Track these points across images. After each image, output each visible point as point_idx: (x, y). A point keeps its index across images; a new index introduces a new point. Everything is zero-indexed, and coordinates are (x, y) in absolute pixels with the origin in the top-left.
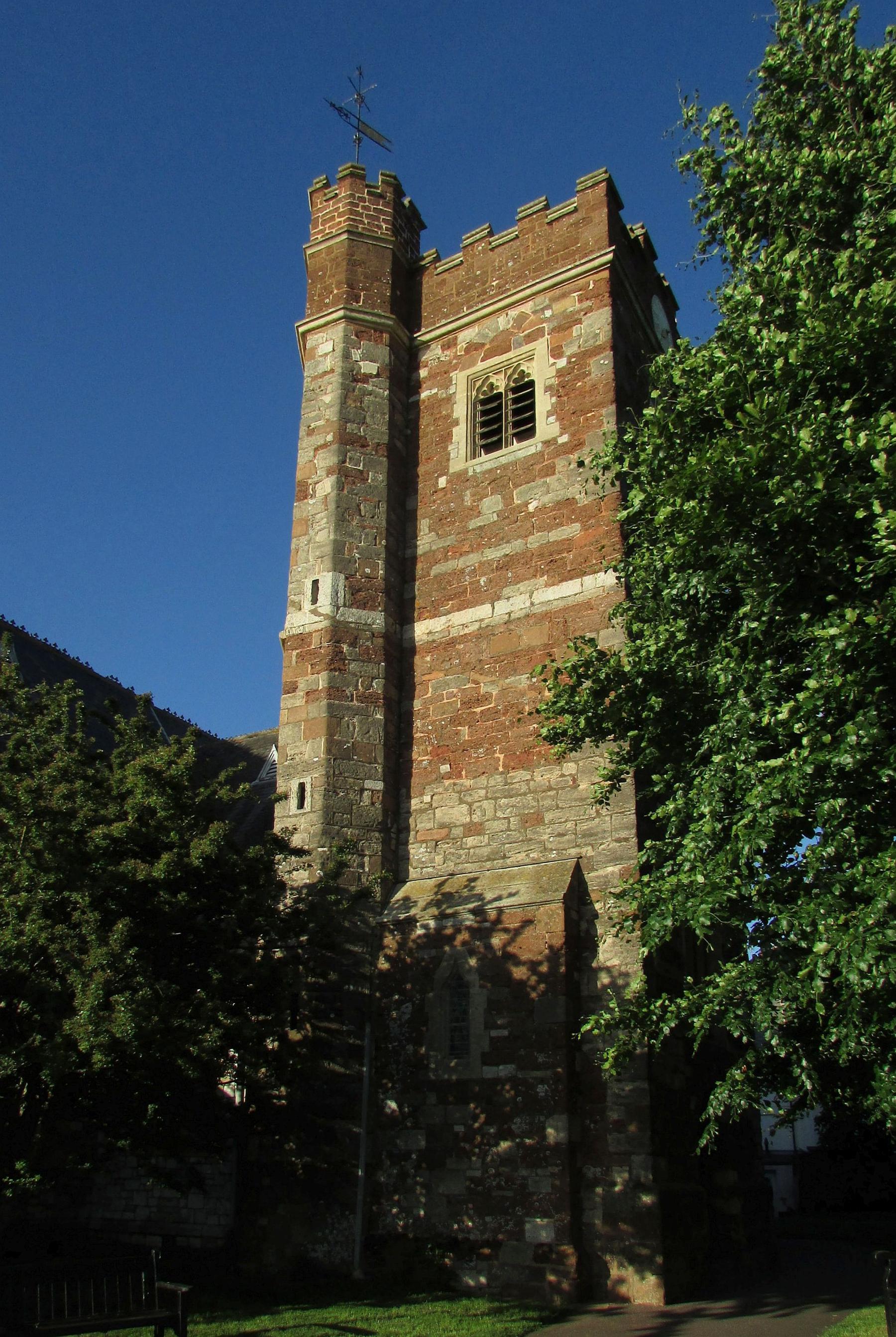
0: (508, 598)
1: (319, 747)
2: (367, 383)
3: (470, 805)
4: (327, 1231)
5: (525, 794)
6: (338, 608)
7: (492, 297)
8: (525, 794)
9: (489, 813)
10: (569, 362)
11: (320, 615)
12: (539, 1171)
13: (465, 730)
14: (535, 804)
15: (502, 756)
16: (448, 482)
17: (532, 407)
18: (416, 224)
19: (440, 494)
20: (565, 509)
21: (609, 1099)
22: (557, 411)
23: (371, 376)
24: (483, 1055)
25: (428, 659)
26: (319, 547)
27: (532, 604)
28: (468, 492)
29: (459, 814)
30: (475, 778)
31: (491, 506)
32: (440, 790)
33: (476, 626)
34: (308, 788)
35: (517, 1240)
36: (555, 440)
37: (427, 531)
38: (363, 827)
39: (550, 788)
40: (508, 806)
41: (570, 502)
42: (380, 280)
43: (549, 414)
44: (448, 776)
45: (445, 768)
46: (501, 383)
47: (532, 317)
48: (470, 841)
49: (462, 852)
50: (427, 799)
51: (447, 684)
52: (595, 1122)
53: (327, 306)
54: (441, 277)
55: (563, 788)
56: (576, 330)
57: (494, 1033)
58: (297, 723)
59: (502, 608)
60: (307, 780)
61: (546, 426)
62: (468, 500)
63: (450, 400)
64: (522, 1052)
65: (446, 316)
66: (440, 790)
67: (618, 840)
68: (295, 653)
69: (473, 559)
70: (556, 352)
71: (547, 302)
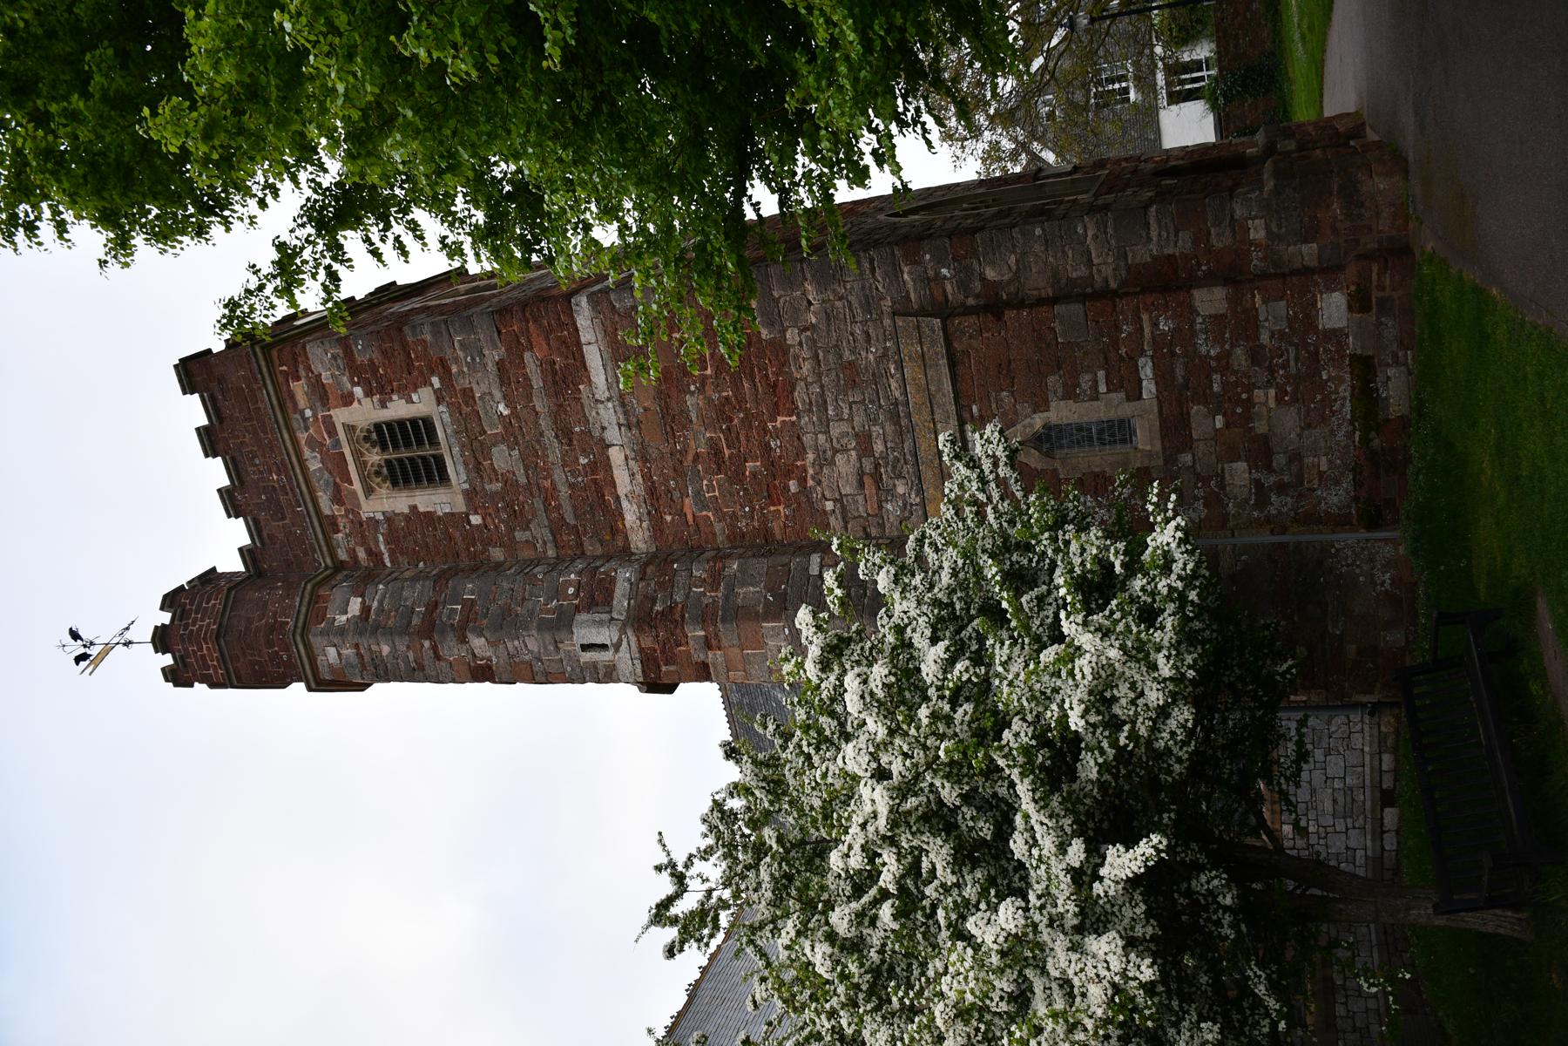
0: (604, 428)
1: (773, 628)
2: (370, 608)
3: (835, 451)
5: (822, 387)
9: (845, 427)
10: (358, 384)
11: (620, 640)
12: (1262, 318)
15: (780, 419)
16: (476, 513)
17: (401, 423)
20: (507, 374)
21: (1169, 251)
22: (406, 393)
23: (363, 603)
24: (1128, 400)
25: (669, 518)
27: (609, 400)
28: (487, 487)
29: (845, 465)
31: (503, 458)
33: (632, 463)
36: (435, 391)
41: (500, 365)
42: (266, 603)
44: (802, 481)
45: (793, 486)
46: (375, 457)
48: (879, 447)
50: (829, 505)
51: (698, 493)
52: (1199, 265)
53: (290, 657)
54: (267, 541)
56: (326, 378)
57: (1103, 388)
58: (746, 660)
59: (613, 435)
61: (422, 404)
63: (390, 518)
64: (1123, 351)
65: (304, 530)
67: (873, 271)
68: (664, 669)
69: (559, 475)
70: (348, 400)
71: (298, 416)
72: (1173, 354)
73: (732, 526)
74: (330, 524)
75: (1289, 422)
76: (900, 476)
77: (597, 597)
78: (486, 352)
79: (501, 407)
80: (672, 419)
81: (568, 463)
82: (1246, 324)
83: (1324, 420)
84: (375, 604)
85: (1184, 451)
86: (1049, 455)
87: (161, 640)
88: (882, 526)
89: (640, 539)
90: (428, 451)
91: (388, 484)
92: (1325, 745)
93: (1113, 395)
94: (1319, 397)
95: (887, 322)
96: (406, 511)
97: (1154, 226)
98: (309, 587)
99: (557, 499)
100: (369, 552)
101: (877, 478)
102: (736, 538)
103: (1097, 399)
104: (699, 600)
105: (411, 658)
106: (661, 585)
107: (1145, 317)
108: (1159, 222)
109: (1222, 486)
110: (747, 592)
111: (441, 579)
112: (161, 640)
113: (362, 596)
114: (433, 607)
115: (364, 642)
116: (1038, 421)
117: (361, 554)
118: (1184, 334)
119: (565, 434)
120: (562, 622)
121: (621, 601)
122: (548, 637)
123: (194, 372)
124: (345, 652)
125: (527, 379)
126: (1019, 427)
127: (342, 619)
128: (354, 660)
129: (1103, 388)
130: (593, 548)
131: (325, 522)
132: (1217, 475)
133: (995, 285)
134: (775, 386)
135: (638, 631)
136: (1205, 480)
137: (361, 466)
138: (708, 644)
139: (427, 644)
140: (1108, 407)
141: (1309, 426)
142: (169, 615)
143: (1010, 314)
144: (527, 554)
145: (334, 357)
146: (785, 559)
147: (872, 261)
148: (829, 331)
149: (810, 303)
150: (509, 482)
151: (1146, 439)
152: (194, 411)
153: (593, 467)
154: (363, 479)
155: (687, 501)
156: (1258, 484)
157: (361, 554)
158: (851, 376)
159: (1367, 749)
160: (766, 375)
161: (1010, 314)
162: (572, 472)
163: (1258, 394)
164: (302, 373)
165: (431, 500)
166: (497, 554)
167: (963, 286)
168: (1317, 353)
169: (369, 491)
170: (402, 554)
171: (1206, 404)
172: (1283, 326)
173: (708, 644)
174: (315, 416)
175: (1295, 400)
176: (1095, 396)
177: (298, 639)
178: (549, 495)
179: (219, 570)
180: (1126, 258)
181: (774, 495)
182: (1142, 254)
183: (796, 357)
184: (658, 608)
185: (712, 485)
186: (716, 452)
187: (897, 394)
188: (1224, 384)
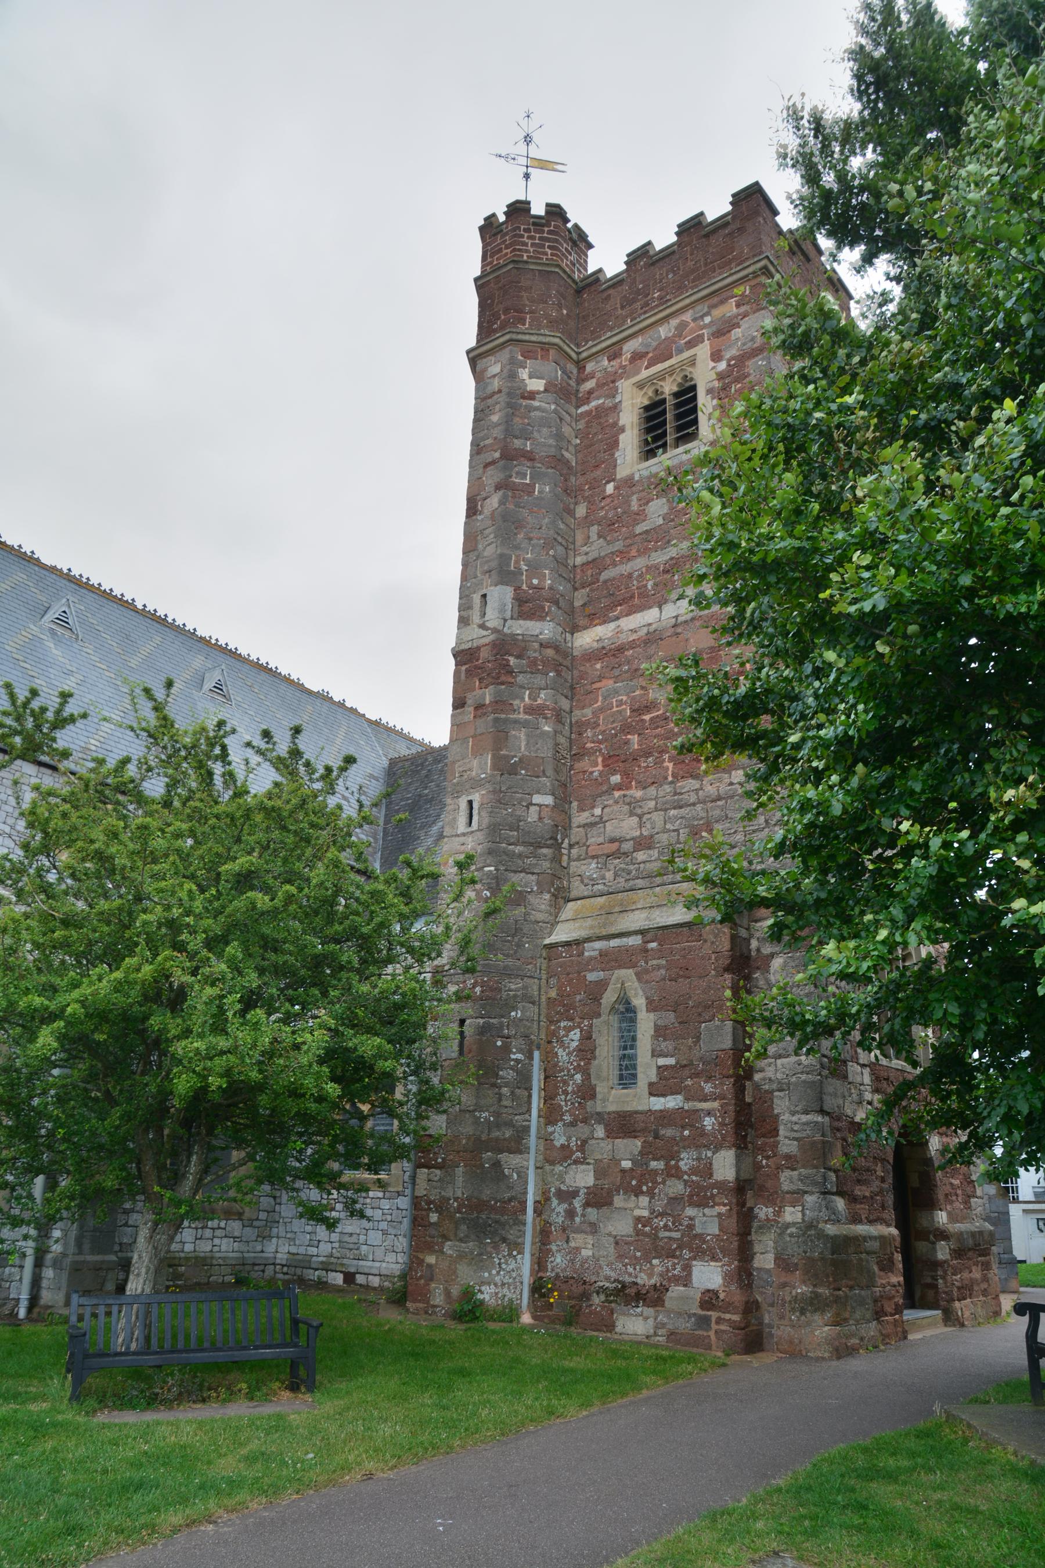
2: (534, 399)
3: (640, 817)
4: (494, 1272)
5: (694, 804)
6: (505, 620)
7: (653, 308)
8: (694, 804)
9: (659, 824)
10: (729, 365)
12: (706, 1210)
13: (634, 739)
14: (704, 815)
15: (671, 765)
16: (616, 488)
17: (694, 410)
18: (582, 246)
19: (608, 500)
21: (782, 1132)
23: (538, 392)
24: (651, 1084)
25: (598, 666)
26: (487, 562)
28: (634, 498)
29: (628, 827)
30: (645, 788)
32: (611, 802)
33: (645, 630)
34: (475, 806)
35: (685, 1286)
37: (595, 537)
38: (531, 844)
39: (719, 798)
40: (676, 818)
42: (546, 302)
44: (618, 787)
45: (616, 779)
46: (669, 388)
47: (692, 324)
48: (641, 856)
49: (631, 867)
50: (598, 811)
51: (616, 692)
52: (768, 1158)
53: (495, 331)
54: (605, 294)
55: (732, 797)
56: (737, 333)
57: (662, 1061)
60: (476, 798)
62: (635, 506)
63: (616, 408)
64: (689, 1082)
65: (611, 329)
66: (611, 802)
69: (640, 563)
70: (716, 357)
71: (706, 310)
72: (683, 1128)
73: (587, 724)
75: (621, 1226)
76: (616, 875)
77: (527, 606)
82: (700, 1198)
83: (620, 1257)
84: (536, 404)
87: (518, 209)
88: (578, 859)
89: (587, 639)
90: (670, 438)
91: (646, 402)
92: (391, 1231)
93: (654, 1071)
94: (638, 1254)
97: (805, 1118)
98: (557, 341)
99: (621, 563)
100: (590, 392)
101: (617, 854)
102: (579, 728)
103: (653, 1056)
104: (516, 697)
105: (487, 442)
106: (533, 663)
107: (716, 1105)
108: (807, 1124)
109: (576, 1162)
110: (520, 737)
111: (558, 462)
113: (546, 390)
114: (530, 457)
115: (502, 398)
116: (639, 1002)
118: (700, 1140)
120: (505, 575)
122: (494, 564)
126: (636, 984)
127: (524, 374)
129: (662, 1061)
130: (580, 598)
131: (616, 348)
132: (585, 1158)
133: (766, 969)
135: (494, 645)
136: (582, 1148)
137: (662, 376)
140: (647, 1070)
141: (617, 1243)
142: (542, 213)
144: (579, 537)
145: (753, 339)
146: (550, 772)
150: (640, 516)
151: (613, 1099)
152: (717, 207)
153: (644, 594)
155: (611, 682)
156: (575, 1194)
157: (590, 385)
159: (384, 1265)
162: (641, 576)
163: (644, 1200)
164: (743, 309)
165: (630, 441)
166: (581, 511)
168: (674, 1256)
169: (640, 386)
170: (587, 423)
171: (641, 1153)
172: (698, 1230)
175: (638, 1233)
176: (655, 1054)
177: (507, 337)
178: (624, 555)
179: (590, 252)
180: (779, 1090)
181: (610, 761)
182: (781, 1105)
183: (720, 780)
184: (512, 661)
186: (649, 707)
188: (655, 1172)
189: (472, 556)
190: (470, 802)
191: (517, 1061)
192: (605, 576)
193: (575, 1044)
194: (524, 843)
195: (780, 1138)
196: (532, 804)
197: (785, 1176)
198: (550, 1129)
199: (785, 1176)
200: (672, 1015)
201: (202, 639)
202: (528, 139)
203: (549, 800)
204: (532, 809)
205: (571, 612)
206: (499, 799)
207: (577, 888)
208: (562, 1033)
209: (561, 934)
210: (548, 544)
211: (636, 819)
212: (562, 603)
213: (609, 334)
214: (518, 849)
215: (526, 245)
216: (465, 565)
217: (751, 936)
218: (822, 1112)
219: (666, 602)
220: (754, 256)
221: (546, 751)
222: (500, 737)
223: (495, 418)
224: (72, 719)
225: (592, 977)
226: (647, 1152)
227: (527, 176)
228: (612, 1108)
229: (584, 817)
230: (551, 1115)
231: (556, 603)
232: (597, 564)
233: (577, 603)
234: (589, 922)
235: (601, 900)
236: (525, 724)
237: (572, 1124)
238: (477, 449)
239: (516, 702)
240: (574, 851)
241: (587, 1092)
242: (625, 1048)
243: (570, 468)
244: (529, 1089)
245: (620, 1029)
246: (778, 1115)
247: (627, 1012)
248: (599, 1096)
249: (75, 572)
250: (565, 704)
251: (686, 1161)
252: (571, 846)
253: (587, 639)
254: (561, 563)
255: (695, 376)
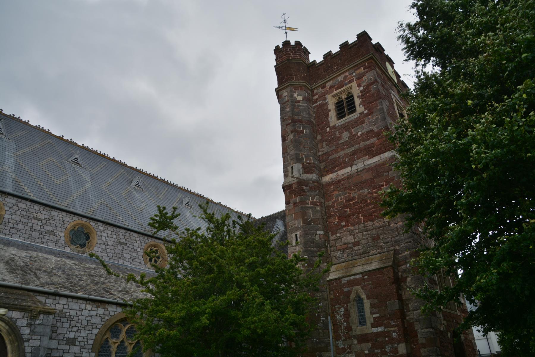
3: (354, 235)
5: (372, 230)
7: (335, 72)
8: (372, 230)
11: (294, 178)
15: (362, 218)
17: (354, 103)
20: (370, 134)
21: (419, 336)
23: (301, 100)
24: (372, 324)
25: (332, 187)
27: (365, 165)
29: (350, 239)
31: (346, 136)
33: (347, 174)
34: (298, 236)
39: (381, 227)
40: (366, 235)
41: (372, 131)
43: (360, 105)
44: (345, 226)
45: (343, 224)
46: (344, 96)
48: (356, 248)
50: (338, 235)
51: (340, 195)
52: (415, 345)
53: (284, 82)
57: (374, 316)
59: (354, 168)
60: (298, 234)
61: (360, 108)
62: (338, 135)
63: (327, 104)
64: (385, 322)
65: (321, 79)
67: (407, 243)
69: (342, 153)
70: (359, 85)
73: (331, 206)
74: (323, 86)
76: (348, 255)
77: (307, 170)
78: (376, 126)
79: (360, 133)
80: (361, 185)
81: (346, 155)
84: (301, 104)
85: (358, 341)
86: (355, 300)
87: (286, 43)
88: (334, 251)
89: (327, 179)
91: (336, 101)
93: (372, 319)
95: (392, 248)
96: (329, 108)
97: (426, 330)
100: (317, 99)
101: (347, 248)
103: (371, 314)
106: (311, 188)
107: (396, 328)
108: (427, 332)
109: (348, 353)
111: (310, 122)
112: (286, 43)
113: (303, 100)
114: (301, 121)
115: (289, 103)
116: (364, 296)
117: (316, 97)
118: (392, 341)
119: (354, 153)
120: (298, 160)
121: (305, 177)
123: (364, 37)
124: (286, 98)
125: (369, 139)
127: (295, 95)
128: (285, 101)
129: (374, 316)
130: (322, 166)
134: (372, 215)
135: (298, 183)
136: (350, 347)
137: (341, 93)
138: (295, 204)
139: (290, 121)
140: (370, 318)
143: (394, 286)
144: (320, 146)
145: (371, 79)
147: (410, 242)
148: (388, 230)
149: (396, 224)
150: (340, 138)
151: (358, 330)
152: (352, 39)
153: (344, 162)
154: (337, 94)
157: (316, 97)
158: (376, 238)
160: (374, 213)
161: (394, 286)
162: (343, 157)
164: (366, 70)
165: (333, 114)
166: (319, 137)
167: (404, 271)
169: (334, 96)
173: (295, 204)
174: (354, 76)
176: (372, 313)
178: (337, 151)
179: (310, 55)
182: (417, 327)
183: (380, 221)
184: (304, 188)
185: (342, 199)
186: (352, 199)
187: (371, 253)
188: (377, 353)
189: (286, 155)
190: (296, 235)
191: (323, 320)
192: (330, 158)
193: (342, 313)
194: (316, 247)
195: (419, 338)
196: (317, 234)
197: (422, 350)
198: (337, 343)
199: (422, 350)
200: (376, 300)
201: (180, 188)
202: (285, 22)
203: (322, 232)
204: (317, 236)
205: (320, 170)
206: (306, 233)
207: (335, 261)
208: (337, 309)
209: (332, 276)
210: (311, 149)
211: (352, 236)
212: (317, 168)
213: (321, 81)
214: (314, 249)
215: (290, 54)
216: (284, 157)
217: (399, 271)
218: (432, 328)
219: (353, 165)
220: (368, 53)
221: (319, 216)
222: (304, 213)
223: (288, 110)
224: (177, 216)
225: (345, 290)
226: (374, 347)
227: (286, 33)
228: (359, 333)
229: (334, 237)
230: (337, 338)
231: (316, 168)
232: (327, 154)
233: (322, 167)
234: (341, 272)
235: (344, 264)
236: (311, 208)
237: (345, 340)
238: (283, 120)
239: (307, 201)
240: (332, 249)
241: (349, 328)
242: (360, 312)
243: (313, 124)
244: (328, 329)
245: (358, 307)
246: (417, 330)
247: (359, 300)
248: (354, 330)
249: (138, 168)
250: (322, 201)
251: (388, 349)
252: (330, 247)
253: (327, 179)
254: (315, 154)
255: (352, 92)
